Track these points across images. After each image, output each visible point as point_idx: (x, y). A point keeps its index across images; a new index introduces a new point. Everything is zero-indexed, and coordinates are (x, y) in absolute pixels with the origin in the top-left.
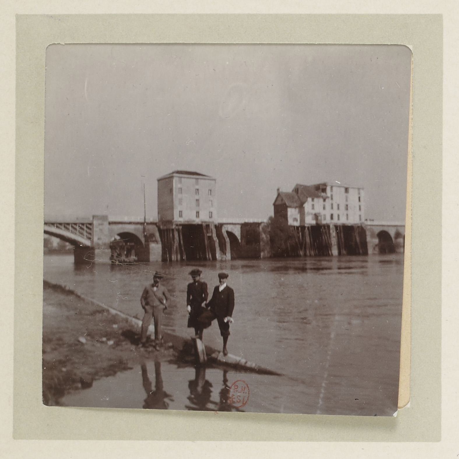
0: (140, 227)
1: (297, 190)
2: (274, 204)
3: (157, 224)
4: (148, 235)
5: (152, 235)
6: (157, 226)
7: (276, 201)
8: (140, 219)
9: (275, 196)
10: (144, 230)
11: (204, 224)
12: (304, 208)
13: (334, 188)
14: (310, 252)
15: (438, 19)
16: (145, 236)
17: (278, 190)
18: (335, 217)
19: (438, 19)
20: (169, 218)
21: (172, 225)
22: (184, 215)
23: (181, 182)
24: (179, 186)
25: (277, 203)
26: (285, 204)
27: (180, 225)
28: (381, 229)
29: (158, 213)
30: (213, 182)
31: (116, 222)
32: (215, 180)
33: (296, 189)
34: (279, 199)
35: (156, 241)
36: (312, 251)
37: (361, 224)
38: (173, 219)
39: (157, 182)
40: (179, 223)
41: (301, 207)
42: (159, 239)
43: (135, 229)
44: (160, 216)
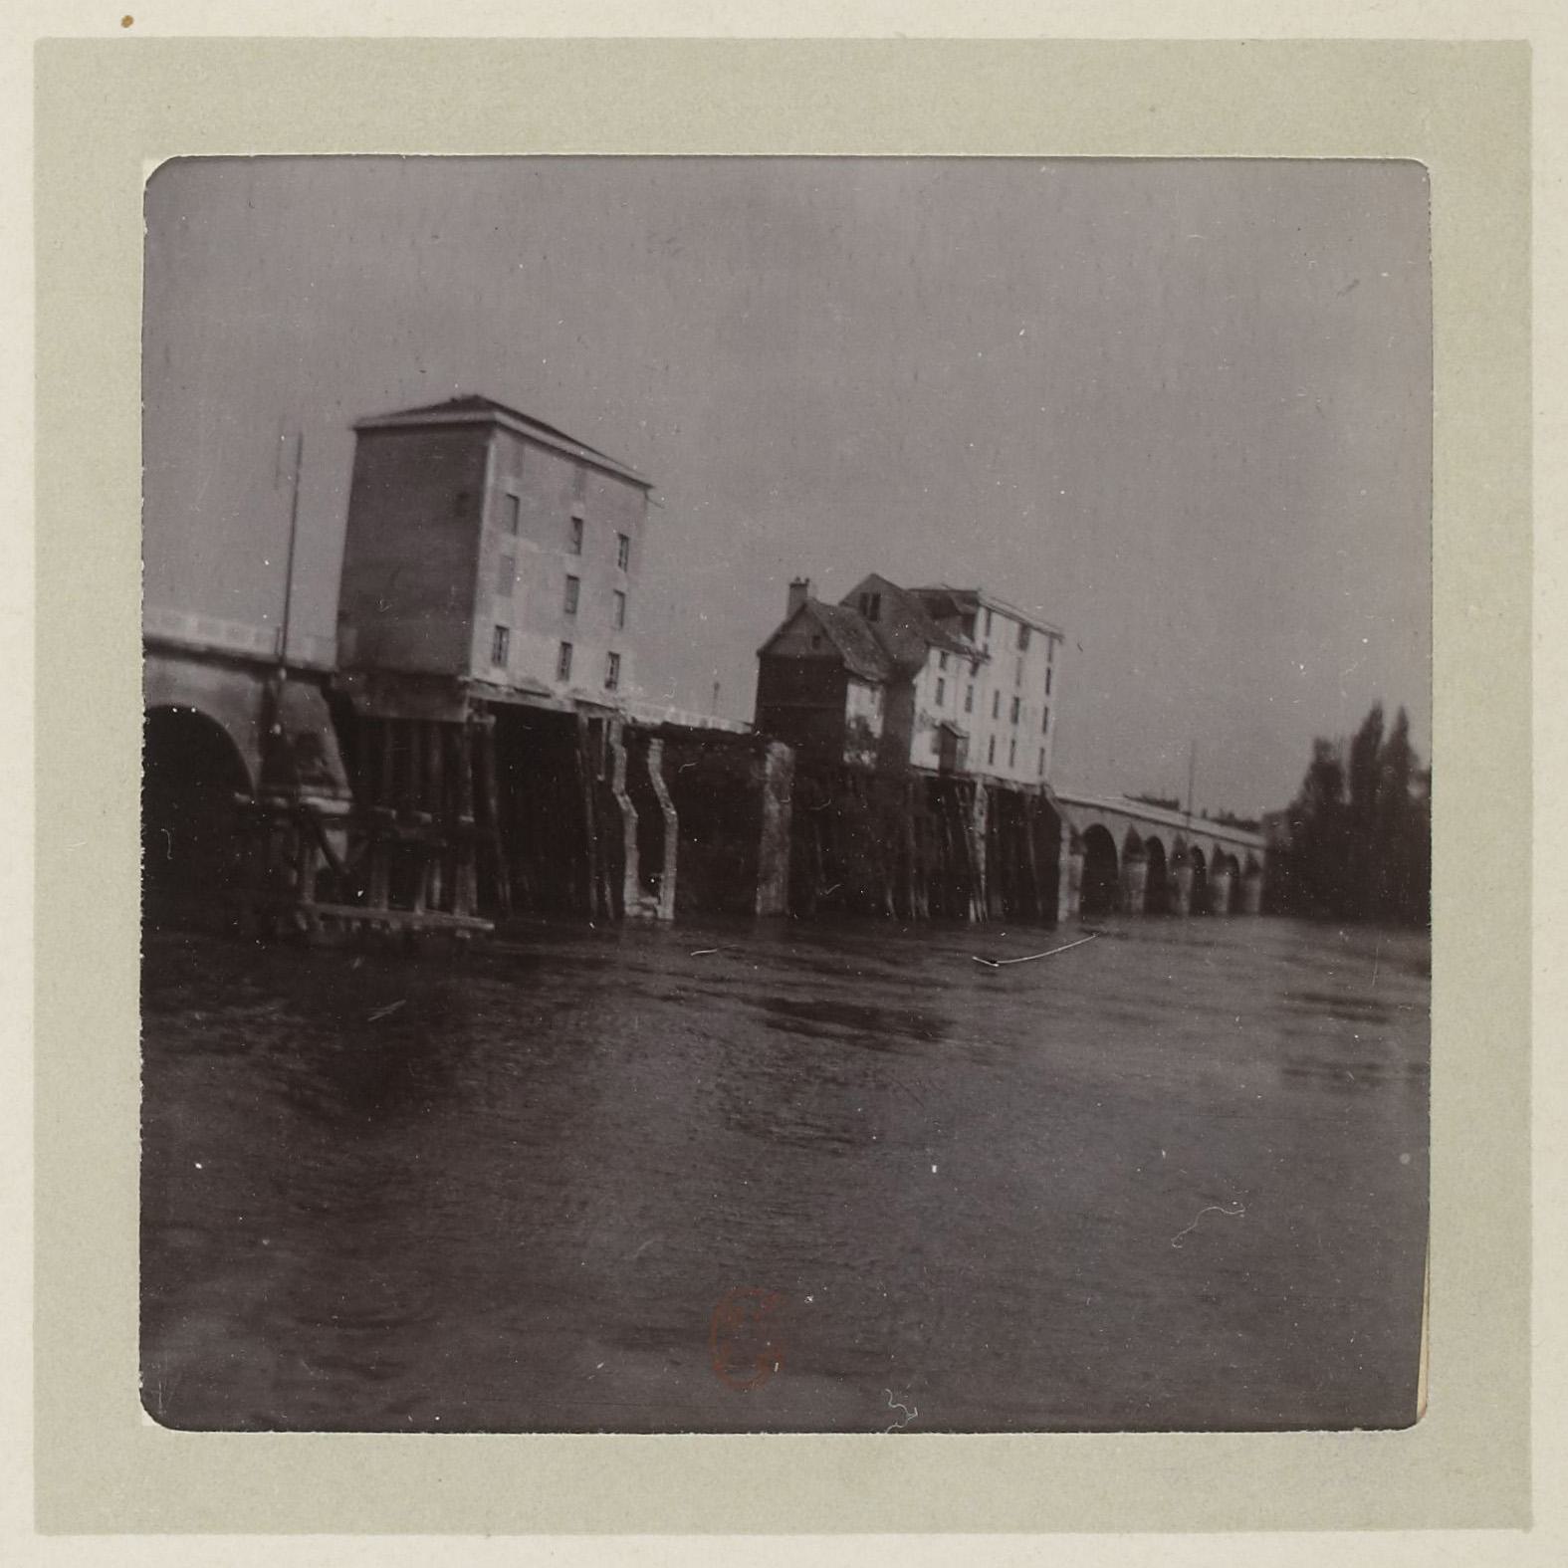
0: (248, 685)
1: (870, 603)
2: (766, 656)
3: (334, 684)
4: (289, 738)
5: (309, 744)
6: (327, 693)
7: (777, 638)
8: (254, 641)
9: (779, 615)
10: (269, 707)
11: (584, 717)
12: (913, 688)
13: (995, 617)
14: (917, 899)
15: (1516, 57)
16: (268, 744)
17: (798, 587)
18: (1002, 753)
19: (1516, 57)
20: (431, 658)
21: (458, 702)
22: (513, 657)
23: (518, 470)
24: (510, 485)
25: (781, 650)
26: (841, 660)
27: (493, 707)
28: (1096, 818)
29: (343, 618)
30: (636, 495)
31: (562, 657)
32: (645, 487)
33: (864, 597)
34: (803, 630)
35: (326, 781)
36: (922, 897)
37: (1042, 786)
38: (465, 667)
39: (351, 439)
40: (488, 695)
41: (898, 683)
42: (341, 775)
43: (227, 697)
44: (352, 634)
